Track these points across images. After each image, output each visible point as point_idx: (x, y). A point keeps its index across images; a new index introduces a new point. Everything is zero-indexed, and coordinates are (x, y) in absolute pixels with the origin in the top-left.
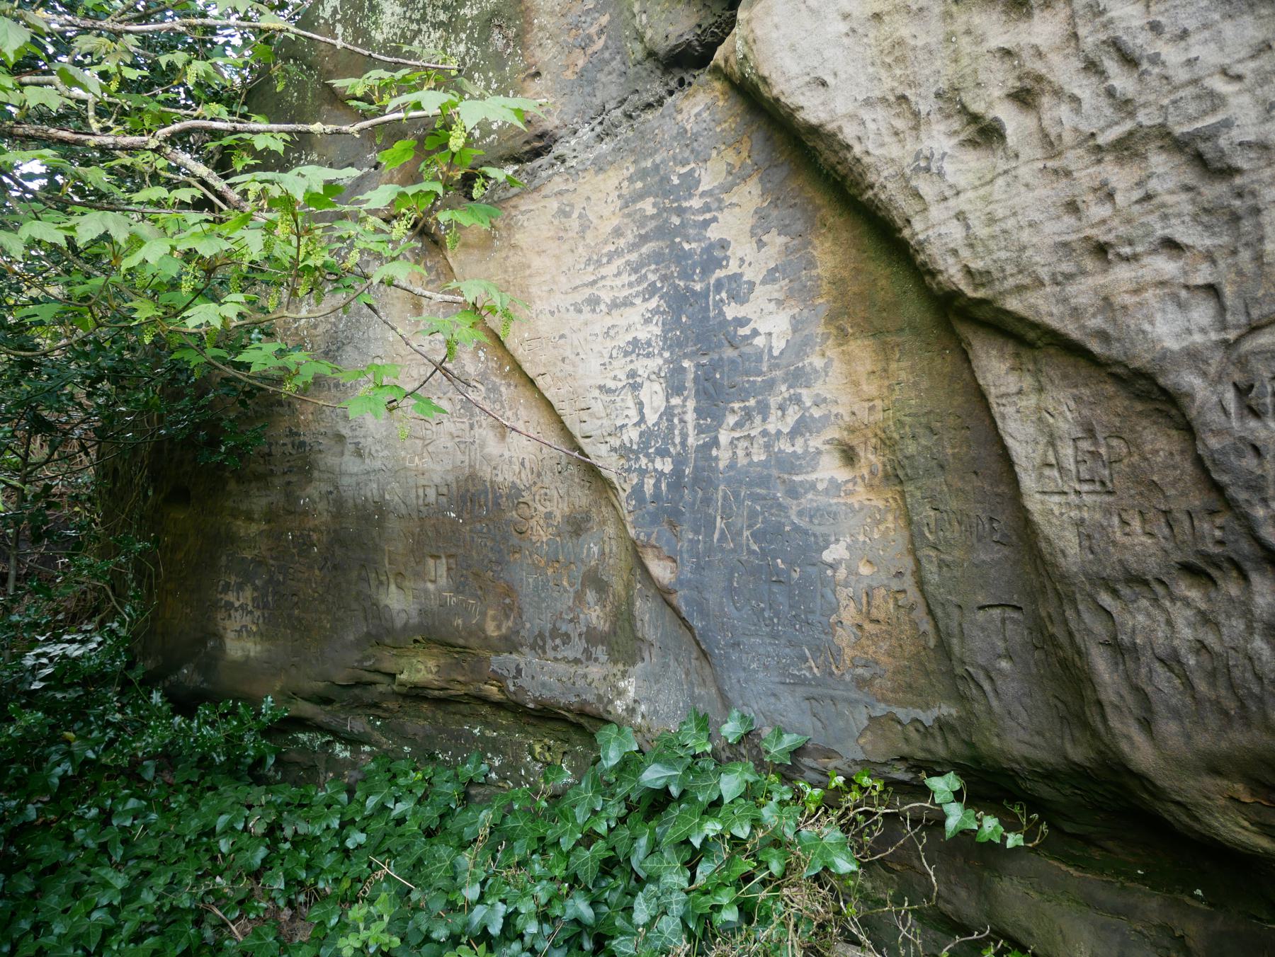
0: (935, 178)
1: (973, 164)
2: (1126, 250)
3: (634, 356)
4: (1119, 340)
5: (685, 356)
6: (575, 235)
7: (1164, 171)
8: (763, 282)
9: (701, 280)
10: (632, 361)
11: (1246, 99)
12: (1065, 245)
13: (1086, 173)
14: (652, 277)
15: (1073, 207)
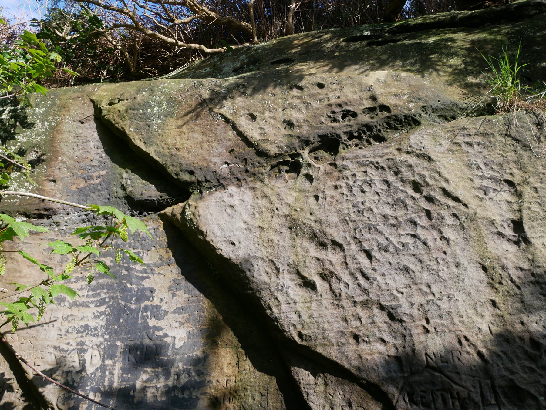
0: (285, 295)
1: (300, 293)
2: (366, 339)
3: (84, 334)
4: (364, 371)
5: (119, 339)
6: (56, 263)
7: (380, 318)
8: (173, 312)
9: (135, 304)
10: (82, 336)
11: (404, 300)
12: (342, 332)
13: (350, 309)
14: (103, 296)
15: (345, 320)
